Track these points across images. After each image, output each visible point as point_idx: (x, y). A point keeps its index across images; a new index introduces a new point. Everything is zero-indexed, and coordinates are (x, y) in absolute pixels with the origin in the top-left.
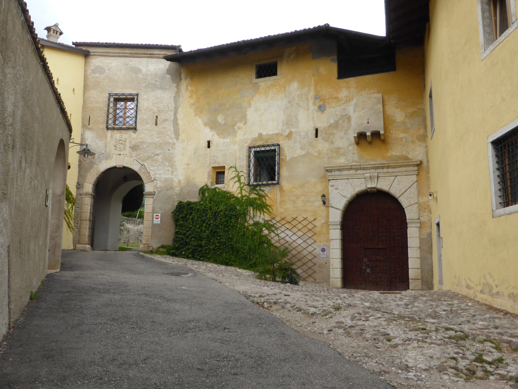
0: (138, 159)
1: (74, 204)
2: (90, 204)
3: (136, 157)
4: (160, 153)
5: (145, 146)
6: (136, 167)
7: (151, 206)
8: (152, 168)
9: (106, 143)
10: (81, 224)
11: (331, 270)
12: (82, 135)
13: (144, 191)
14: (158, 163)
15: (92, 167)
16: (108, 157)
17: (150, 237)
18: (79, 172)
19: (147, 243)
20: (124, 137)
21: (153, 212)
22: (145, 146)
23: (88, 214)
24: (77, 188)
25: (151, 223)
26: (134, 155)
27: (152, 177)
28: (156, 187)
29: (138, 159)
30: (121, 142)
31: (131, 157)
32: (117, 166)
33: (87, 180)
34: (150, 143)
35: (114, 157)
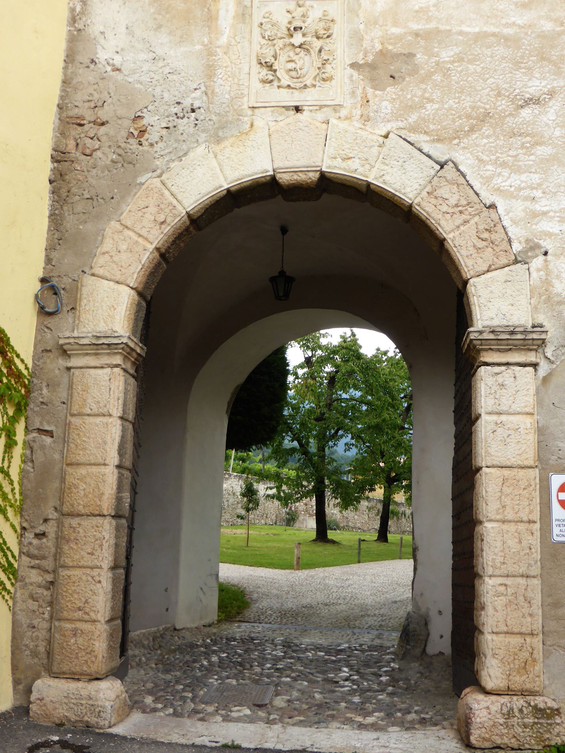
0: (413, 129)
1: (20, 408)
2: (117, 411)
3: (397, 117)
4: (552, 94)
5: (446, 55)
6: (402, 178)
7: (527, 422)
8: (508, 180)
9: (210, 52)
10: (60, 539)
11: (536, 570)
12: (73, 20)
13: (288, 365)
14: (542, 151)
15: (130, 187)
16: (223, 130)
17: (537, 642)
18: (56, 220)
19: (518, 681)
20: (315, 14)
21: (545, 463)
22: (446, 55)
23: (111, 476)
24: (43, 312)
25: (535, 541)
26: (386, 107)
27: (513, 231)
28: (544, 295)
29: (413, 129)
30: (298, 39)
31: (366, 119)
32: (284, 178)
33: (101, 260)
34: (479, 37)
35: (258, 123)
